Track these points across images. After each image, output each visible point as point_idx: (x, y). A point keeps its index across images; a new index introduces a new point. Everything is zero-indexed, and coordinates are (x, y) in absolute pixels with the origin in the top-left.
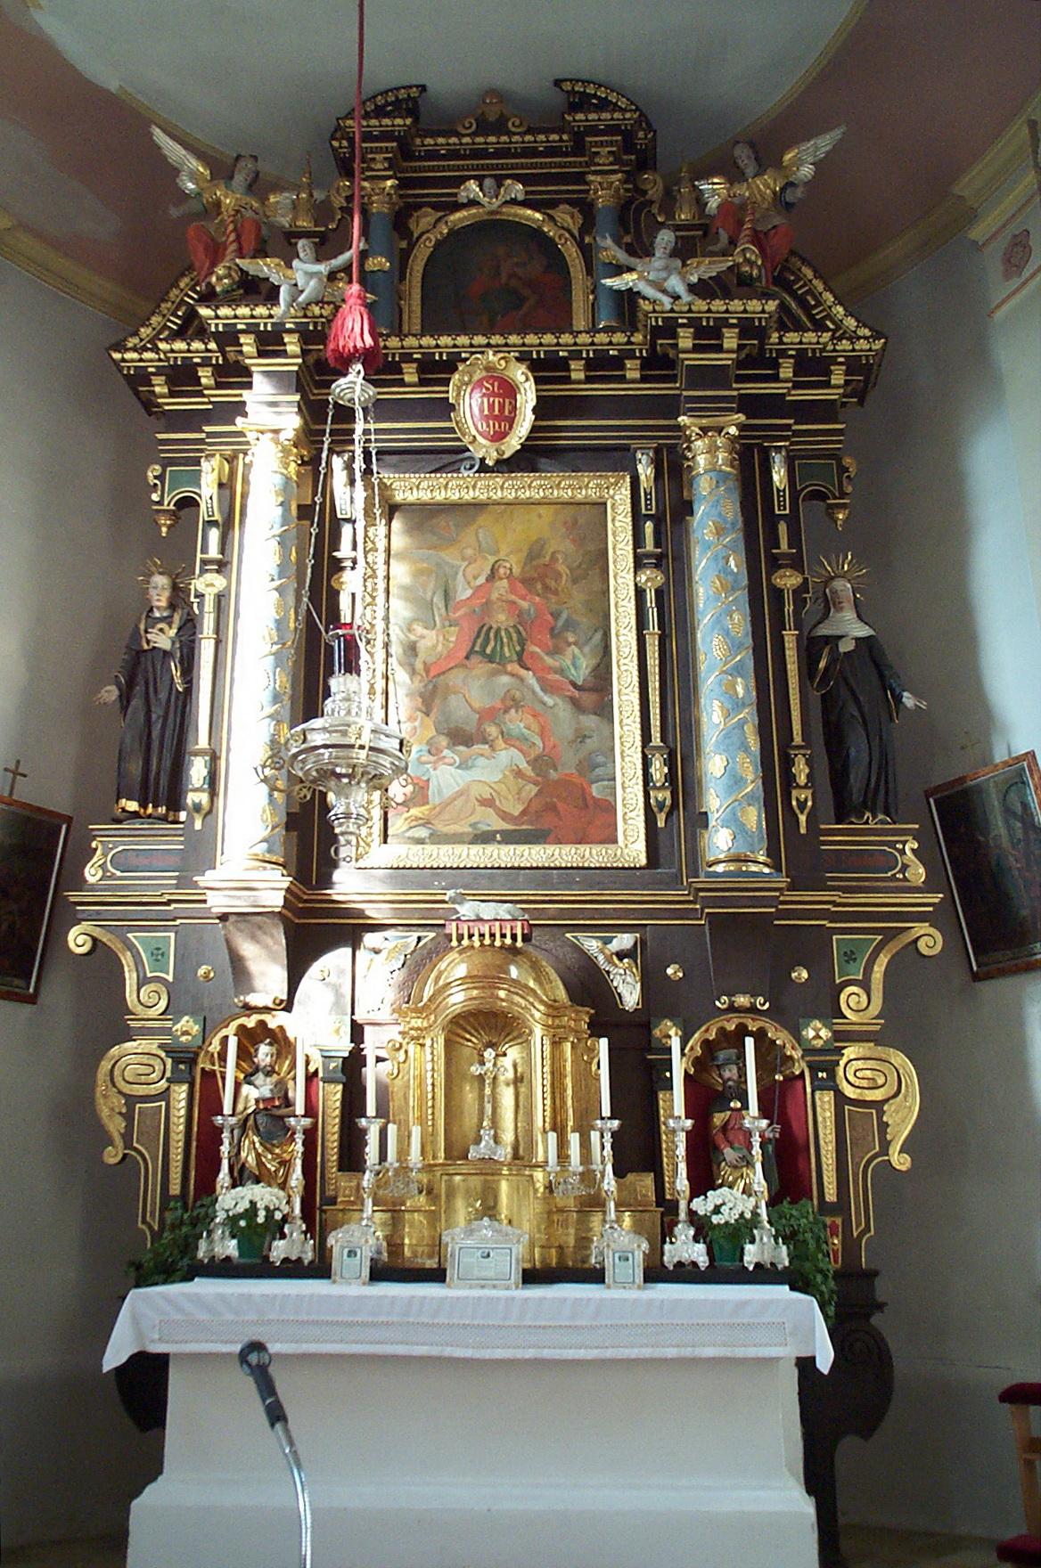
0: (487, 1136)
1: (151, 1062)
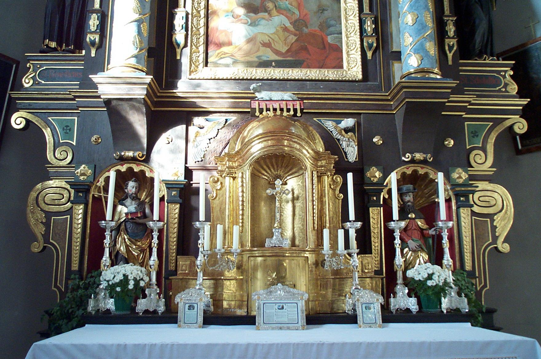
0: (276, 234)
1: (62, 192)
